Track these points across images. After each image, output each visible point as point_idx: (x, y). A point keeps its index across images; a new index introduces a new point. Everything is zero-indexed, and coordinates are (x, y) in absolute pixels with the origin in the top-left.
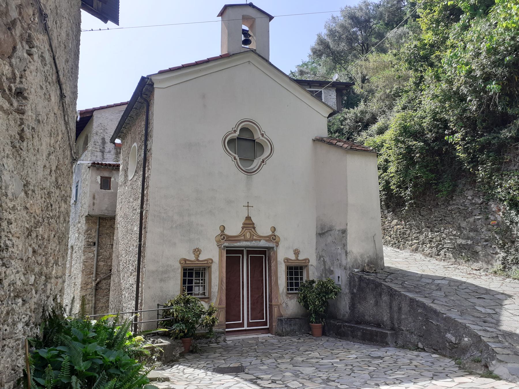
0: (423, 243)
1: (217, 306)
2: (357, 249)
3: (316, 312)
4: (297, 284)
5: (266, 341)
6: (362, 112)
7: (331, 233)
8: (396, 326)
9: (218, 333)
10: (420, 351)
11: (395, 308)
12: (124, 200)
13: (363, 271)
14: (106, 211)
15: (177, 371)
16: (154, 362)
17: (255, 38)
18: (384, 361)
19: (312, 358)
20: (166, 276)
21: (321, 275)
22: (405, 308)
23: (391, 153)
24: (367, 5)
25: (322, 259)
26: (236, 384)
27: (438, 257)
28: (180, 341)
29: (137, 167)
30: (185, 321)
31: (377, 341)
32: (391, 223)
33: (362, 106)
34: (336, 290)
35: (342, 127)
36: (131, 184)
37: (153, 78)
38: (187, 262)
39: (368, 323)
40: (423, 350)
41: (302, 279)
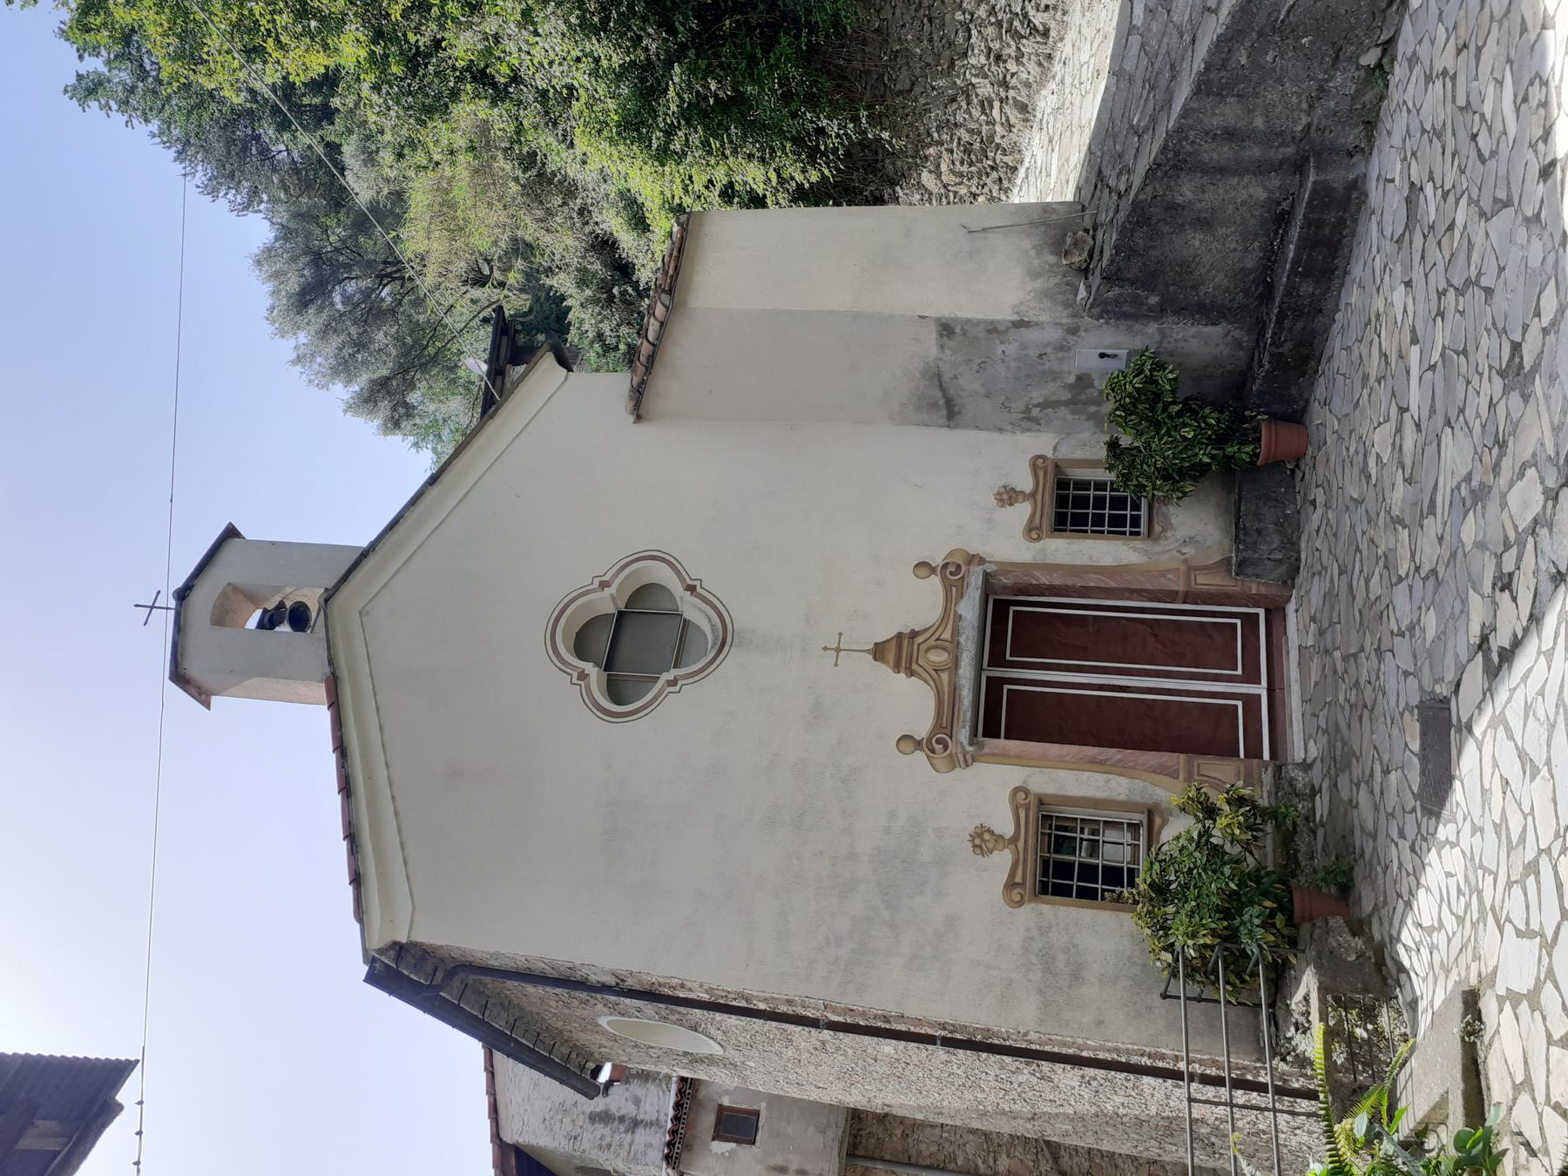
0: (1004, 84)
1: (1180, 784)
2: (1005, 286)
3: (1220, 440)
4: (1118, 503)
5: (1313, 619)
6: (582, 282)
7: (946, 377)
8: (1290, 150)
9: (1277, 787)
10: (1393, 59)
11: (1226, 152)
12: (792, 1077)
13: (1085, 272)
14: (831, 1133)
15: (1425, 952)
16: (1378, 1032)
17: (288, 590)
18: (1431, 179)
19: (1398, 448)
20: (1061, 957)
21: (1090, 417)
22: (1228, 114)
23: (705, 171)
24: (268, 254)
25: (1035, 412)
26: (1507, 729)
27: (1053, 33)
28: (1305, 929)
29: (680, 1022)
30: (1231, 907)
31: (1342, 223)
32: (931, 194)
33: (563, 283)
34: (1148, 367)
35: (622, 347)
36: (737, 1048)
37: (377, 942)
38: (1018, 879)
39: (1271, 258)
40: (1388, 46)
41: (1100, 486)
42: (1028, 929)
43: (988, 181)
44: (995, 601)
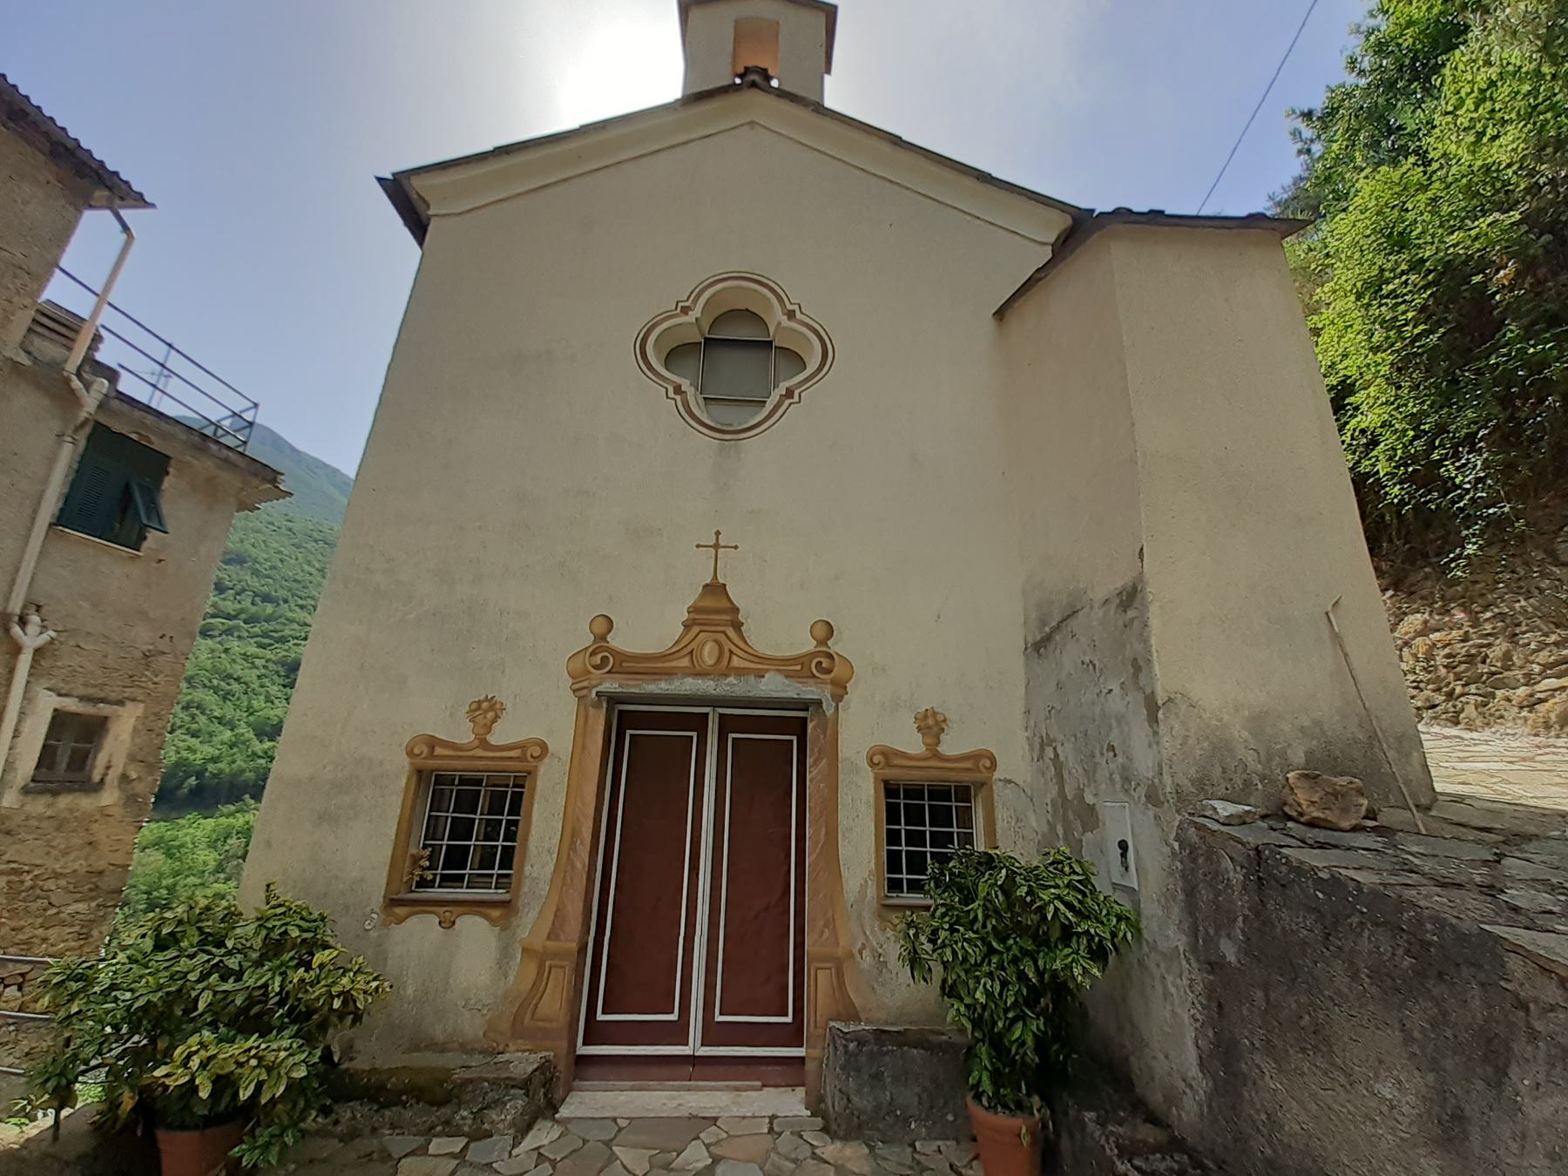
7: (1073, 624)
21: (1052, 826)
25: (1049, 752)
38: (438, 751)
41: (968, 839)
42: (381, 763)
43: (1427, 693)
44: (805, 719)
